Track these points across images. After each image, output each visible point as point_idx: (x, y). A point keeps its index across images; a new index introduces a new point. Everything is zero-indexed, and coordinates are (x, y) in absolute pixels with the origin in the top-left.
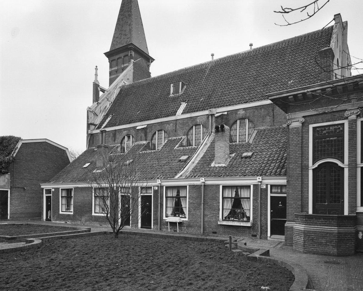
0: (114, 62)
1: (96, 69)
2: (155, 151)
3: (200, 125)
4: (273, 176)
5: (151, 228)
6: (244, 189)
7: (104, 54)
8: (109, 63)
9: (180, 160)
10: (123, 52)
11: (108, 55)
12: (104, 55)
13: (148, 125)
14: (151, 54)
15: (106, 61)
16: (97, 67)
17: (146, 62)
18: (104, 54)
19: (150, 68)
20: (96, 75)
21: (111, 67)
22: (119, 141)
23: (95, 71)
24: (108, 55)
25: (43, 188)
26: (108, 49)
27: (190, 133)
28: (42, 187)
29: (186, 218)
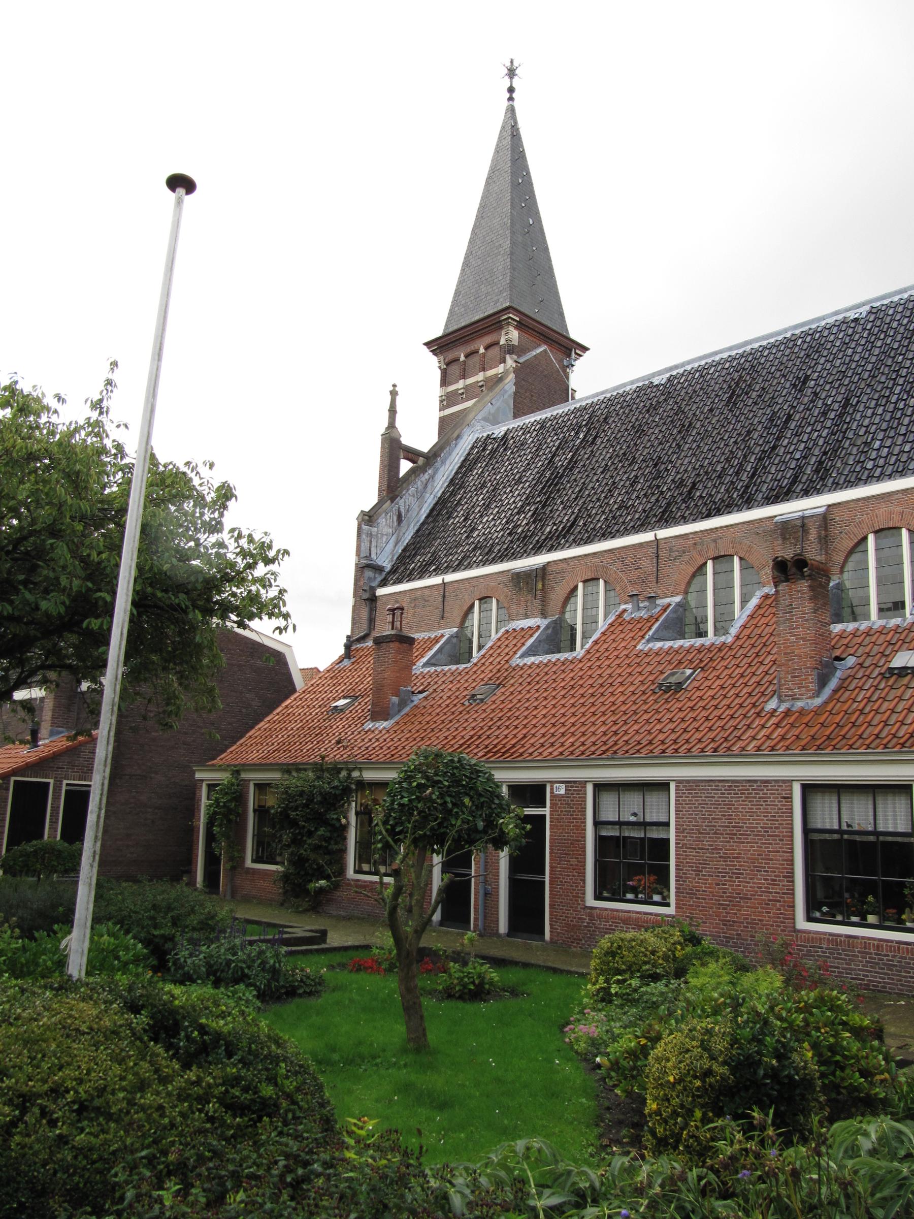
0: (455, 369)
1: (394, 394)
2: (699, 642)
3: (899, 528)
4: (878, 750)
5: (543, 939)
6: (823, 799)
7: (426, 344)
8: (439, 372)
9: (891, 670)
10: (481, 336)
11: (438, 346)
12: (425, 347)
13: (829, 506)
14: (575, 333)
15: (432, 365)
16: (394, 386)
17: (560, 355)
18: (426, 344)
19: (572, 377)
20: (393, 411)
21: (445, 381)
22: (457, 615)
23: (389, 398)
24: (438, 346)
25: (202, 781)
26: (437, 331)
27: (693, 588)
28: (198, 776)
29: (668, 905)
